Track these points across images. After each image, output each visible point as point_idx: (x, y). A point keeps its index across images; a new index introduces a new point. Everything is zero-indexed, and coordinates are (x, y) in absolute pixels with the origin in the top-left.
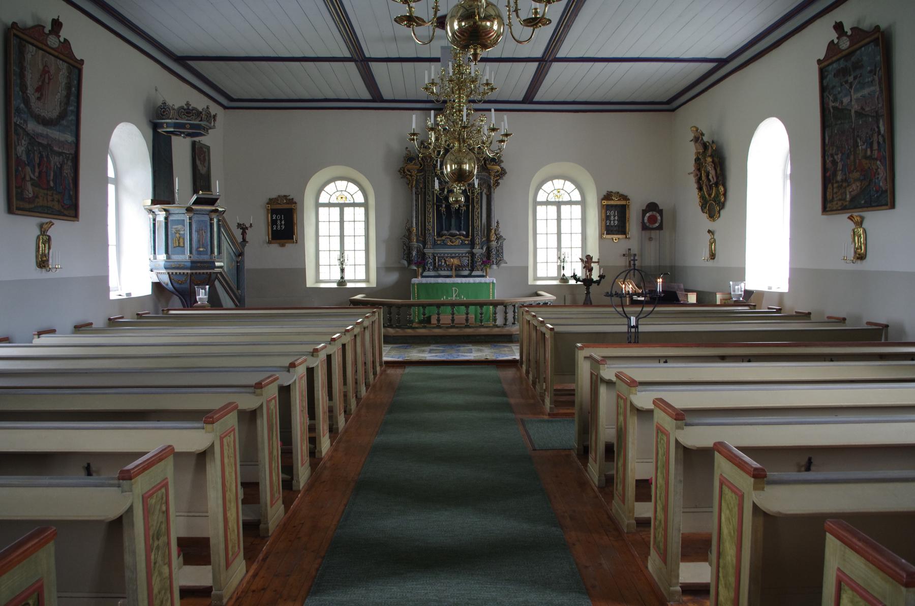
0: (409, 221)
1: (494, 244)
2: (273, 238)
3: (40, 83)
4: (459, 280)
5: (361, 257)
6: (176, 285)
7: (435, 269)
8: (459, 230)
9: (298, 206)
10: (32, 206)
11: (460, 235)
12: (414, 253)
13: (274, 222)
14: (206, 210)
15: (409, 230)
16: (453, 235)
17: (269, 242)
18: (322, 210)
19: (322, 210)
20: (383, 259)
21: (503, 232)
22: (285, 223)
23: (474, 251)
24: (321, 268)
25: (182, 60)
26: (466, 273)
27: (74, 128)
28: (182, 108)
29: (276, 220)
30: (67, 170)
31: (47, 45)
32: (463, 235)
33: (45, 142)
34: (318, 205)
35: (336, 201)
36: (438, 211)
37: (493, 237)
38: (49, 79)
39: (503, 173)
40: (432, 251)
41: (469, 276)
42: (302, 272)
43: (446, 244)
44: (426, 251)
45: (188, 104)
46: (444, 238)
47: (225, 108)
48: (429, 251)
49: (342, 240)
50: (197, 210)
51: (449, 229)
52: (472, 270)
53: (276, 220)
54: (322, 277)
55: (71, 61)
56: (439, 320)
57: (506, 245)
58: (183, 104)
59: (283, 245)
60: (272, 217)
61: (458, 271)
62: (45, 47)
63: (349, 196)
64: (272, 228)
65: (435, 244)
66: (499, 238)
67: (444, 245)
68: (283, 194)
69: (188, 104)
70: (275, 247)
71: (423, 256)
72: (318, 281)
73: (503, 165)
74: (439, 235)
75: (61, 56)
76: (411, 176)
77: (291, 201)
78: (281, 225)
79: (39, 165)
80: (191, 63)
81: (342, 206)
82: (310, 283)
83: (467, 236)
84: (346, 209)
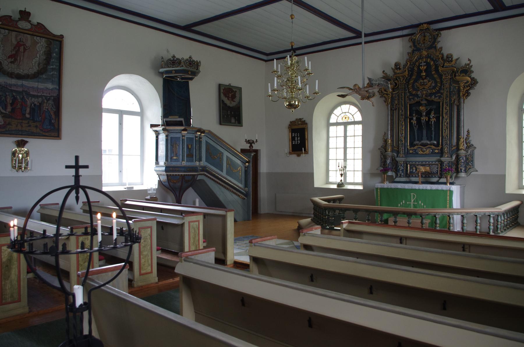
0: (385, 134)
1: (462, 153)
2: (292, 151)
3: (14, 52)
4: (428, 187)
5: (359, 165)
6: (171, 184)
7: (407, 175)
8: (429, 138)
9: (309, 126)
10: (4, 130)
11: (431, 145)
12: (388, 161)
13: (293, 139)
14: (177, 130)
15: (386, 141)
16: (424, 145)
17: (290, 153)
18: (332, 128)
19: (332, 128)
20: (368, 166)
21: (474, 140)
22: (300, 139)
23: (443, 159)
24: (330, 173)
25: (188, 28)
26: (435, 180)
27: (57, 80)
28: (170, 60)
29: (295, 137)
30: (48, 106)
31: (20, 28)
32: (434, 145)
33: (20, 89)
34: (329, 125)
35: (341, 121)
36: (411, 124)
37: (463, 146)
38: (25, 50)
39: (474, 83)
40: (403, 159)
41: (437, 183)
42: (311, 176)
43: (417, 153)
44: (398, 159)
45: (174, 57)
46: (415, 148)
47: (266, 61)
48: (401, 159)
49: (342, 151)
50: (171, 130)
51: (420, 139)
52: (440, 178)
53: (295, 137)
54: (331, 180)
55: (48, 37)
56: (395, 222)
57: (476, 152)
58: (186, 57)
59: (299, 155)
60: (292, 135)
61: (427, 178)
62: (16, 29)
63: (351, 117)
64: (292, 143)
65: (407, 154)
66: (469, 146)
67: (416, 154)
68: (299, 117)
69: (190, 57)
70: (294, 157)
71: (395, 163)
72: (328, 183)
73: (473, 75)
74: (412, 145)
75: (37, 34)
76: (387, 94)
77: (304, 123)
78: (298, 141)
79: (12, 104)
80: (196, 28)
81: (346, 124)
82: (319, 182)
83: (438, 145)
84: (125, 117)
